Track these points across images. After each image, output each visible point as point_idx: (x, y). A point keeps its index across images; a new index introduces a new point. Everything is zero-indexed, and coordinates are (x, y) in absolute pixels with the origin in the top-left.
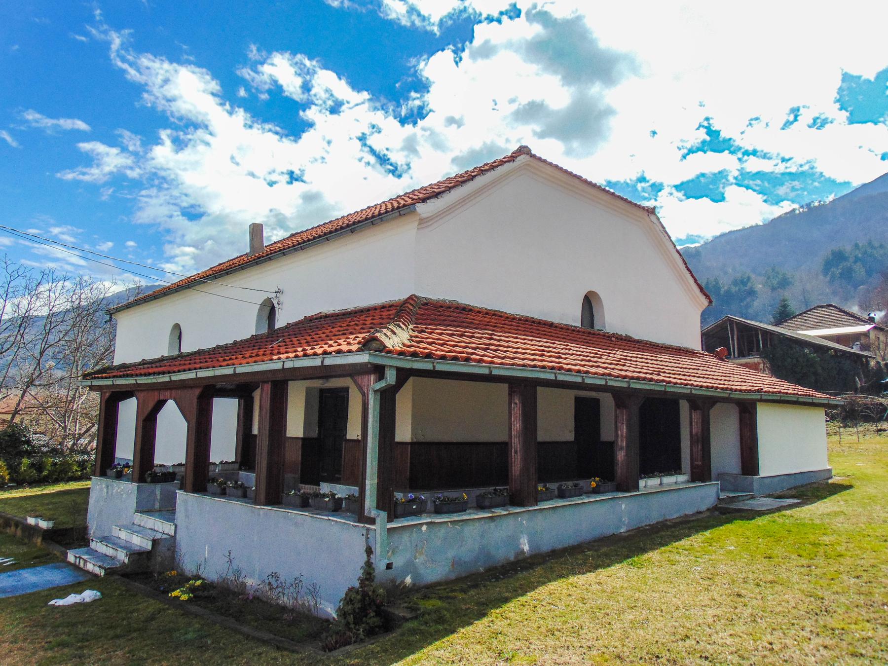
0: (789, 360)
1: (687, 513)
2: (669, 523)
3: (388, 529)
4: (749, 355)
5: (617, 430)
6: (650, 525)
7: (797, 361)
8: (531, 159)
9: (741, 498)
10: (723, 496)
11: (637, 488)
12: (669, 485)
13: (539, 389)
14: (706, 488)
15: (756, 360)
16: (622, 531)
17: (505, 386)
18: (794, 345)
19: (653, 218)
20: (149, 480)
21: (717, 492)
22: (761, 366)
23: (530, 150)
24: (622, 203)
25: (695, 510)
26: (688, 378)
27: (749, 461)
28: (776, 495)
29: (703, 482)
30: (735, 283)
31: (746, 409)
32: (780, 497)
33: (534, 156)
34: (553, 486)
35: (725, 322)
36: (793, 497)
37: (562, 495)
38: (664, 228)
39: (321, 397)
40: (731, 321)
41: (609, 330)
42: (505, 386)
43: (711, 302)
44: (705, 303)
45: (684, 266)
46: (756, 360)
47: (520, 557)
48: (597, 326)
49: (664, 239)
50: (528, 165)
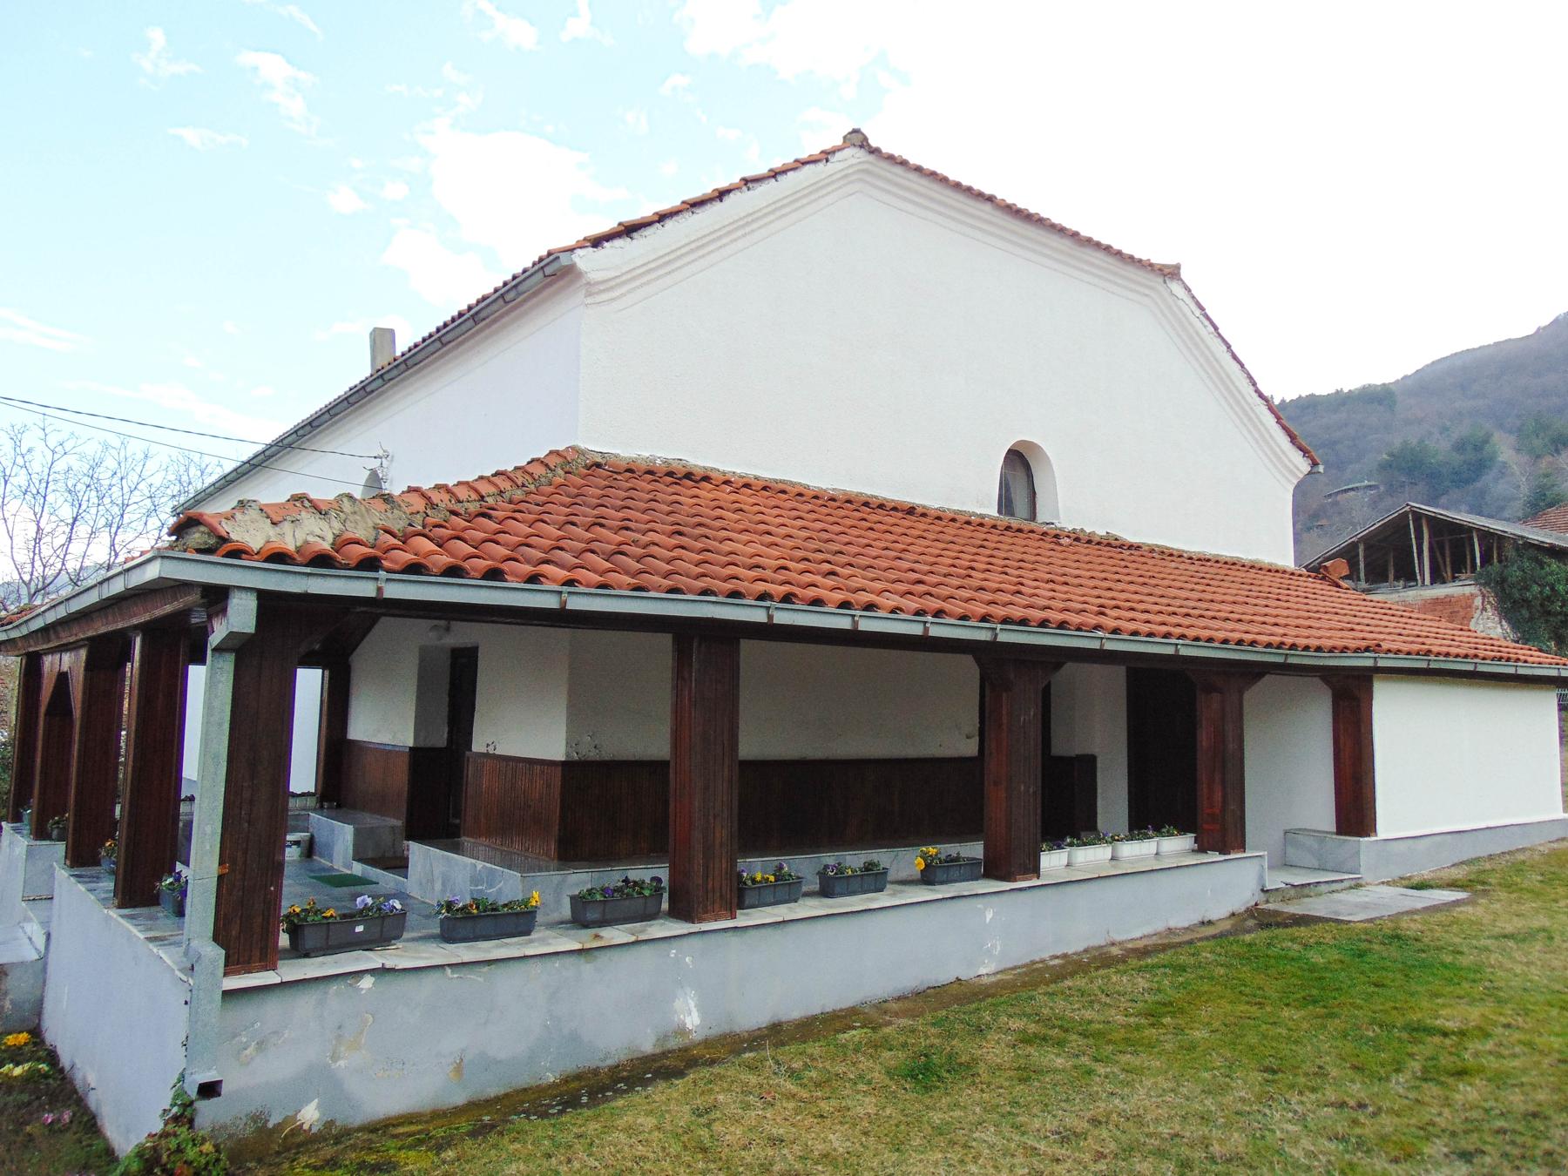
0: (1536, 588)
1: (1173, 924)
2: (1115, 951)
3: (226, 993)
4: (1454, 579)
5: (1101, 732)
6: (1065, 956)
7: (1553, 589)
8: (871, 158)
9: (1323, 888)
10: (1276, 881)
11: (1035, 870)
12: (1141, 859)
13: (746, 646)
14: (507, 983)
15: (1468, 590)
16: (983, 971)
17: (665, 640)
18: (1547, 560)
19: (1175, 287)
20: (55, 833)
21: (1261, 878)
22: (1478, 601)
23: (866, 139)
24: (1100, 255)
25: (1195, 919)
26: (1187, 621)
27: (1355, 809)
28: (1415, 881)
29: (1222, 852)
30: (1460, 447)
31: (1350, 694)
32: (1421, 886)
33: (875, 151)
34: (804, 866)
35: (1405, 514)
36: (1452, 885)
37: (827, 889)
38: (1202, 309)
39: (453, 666)
40: (1418, 517)
41: (1067, 523)
42: (665, 640)
43: (1315, 464)
44: (1304, 466)
45: (1252, 388)
46: (1468, 590)
47: (673, 1044)
48: (1043, 516)
49: (1203, 332)
50: (866, 171)
